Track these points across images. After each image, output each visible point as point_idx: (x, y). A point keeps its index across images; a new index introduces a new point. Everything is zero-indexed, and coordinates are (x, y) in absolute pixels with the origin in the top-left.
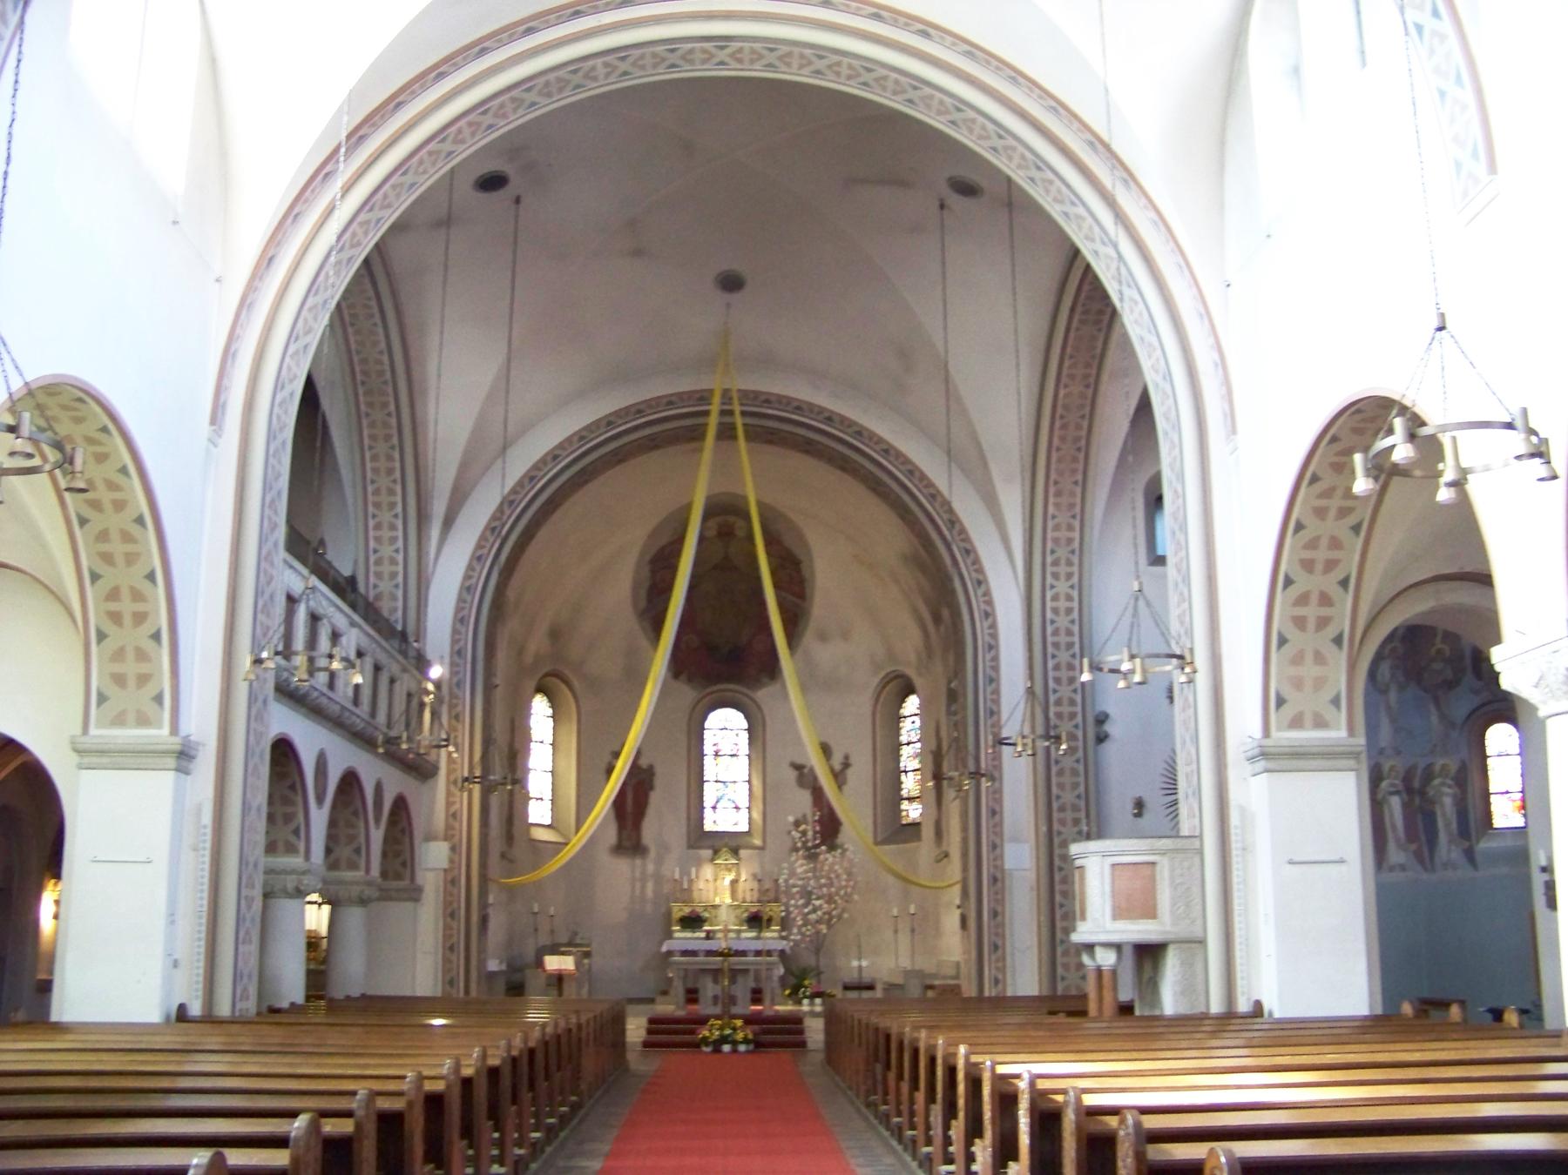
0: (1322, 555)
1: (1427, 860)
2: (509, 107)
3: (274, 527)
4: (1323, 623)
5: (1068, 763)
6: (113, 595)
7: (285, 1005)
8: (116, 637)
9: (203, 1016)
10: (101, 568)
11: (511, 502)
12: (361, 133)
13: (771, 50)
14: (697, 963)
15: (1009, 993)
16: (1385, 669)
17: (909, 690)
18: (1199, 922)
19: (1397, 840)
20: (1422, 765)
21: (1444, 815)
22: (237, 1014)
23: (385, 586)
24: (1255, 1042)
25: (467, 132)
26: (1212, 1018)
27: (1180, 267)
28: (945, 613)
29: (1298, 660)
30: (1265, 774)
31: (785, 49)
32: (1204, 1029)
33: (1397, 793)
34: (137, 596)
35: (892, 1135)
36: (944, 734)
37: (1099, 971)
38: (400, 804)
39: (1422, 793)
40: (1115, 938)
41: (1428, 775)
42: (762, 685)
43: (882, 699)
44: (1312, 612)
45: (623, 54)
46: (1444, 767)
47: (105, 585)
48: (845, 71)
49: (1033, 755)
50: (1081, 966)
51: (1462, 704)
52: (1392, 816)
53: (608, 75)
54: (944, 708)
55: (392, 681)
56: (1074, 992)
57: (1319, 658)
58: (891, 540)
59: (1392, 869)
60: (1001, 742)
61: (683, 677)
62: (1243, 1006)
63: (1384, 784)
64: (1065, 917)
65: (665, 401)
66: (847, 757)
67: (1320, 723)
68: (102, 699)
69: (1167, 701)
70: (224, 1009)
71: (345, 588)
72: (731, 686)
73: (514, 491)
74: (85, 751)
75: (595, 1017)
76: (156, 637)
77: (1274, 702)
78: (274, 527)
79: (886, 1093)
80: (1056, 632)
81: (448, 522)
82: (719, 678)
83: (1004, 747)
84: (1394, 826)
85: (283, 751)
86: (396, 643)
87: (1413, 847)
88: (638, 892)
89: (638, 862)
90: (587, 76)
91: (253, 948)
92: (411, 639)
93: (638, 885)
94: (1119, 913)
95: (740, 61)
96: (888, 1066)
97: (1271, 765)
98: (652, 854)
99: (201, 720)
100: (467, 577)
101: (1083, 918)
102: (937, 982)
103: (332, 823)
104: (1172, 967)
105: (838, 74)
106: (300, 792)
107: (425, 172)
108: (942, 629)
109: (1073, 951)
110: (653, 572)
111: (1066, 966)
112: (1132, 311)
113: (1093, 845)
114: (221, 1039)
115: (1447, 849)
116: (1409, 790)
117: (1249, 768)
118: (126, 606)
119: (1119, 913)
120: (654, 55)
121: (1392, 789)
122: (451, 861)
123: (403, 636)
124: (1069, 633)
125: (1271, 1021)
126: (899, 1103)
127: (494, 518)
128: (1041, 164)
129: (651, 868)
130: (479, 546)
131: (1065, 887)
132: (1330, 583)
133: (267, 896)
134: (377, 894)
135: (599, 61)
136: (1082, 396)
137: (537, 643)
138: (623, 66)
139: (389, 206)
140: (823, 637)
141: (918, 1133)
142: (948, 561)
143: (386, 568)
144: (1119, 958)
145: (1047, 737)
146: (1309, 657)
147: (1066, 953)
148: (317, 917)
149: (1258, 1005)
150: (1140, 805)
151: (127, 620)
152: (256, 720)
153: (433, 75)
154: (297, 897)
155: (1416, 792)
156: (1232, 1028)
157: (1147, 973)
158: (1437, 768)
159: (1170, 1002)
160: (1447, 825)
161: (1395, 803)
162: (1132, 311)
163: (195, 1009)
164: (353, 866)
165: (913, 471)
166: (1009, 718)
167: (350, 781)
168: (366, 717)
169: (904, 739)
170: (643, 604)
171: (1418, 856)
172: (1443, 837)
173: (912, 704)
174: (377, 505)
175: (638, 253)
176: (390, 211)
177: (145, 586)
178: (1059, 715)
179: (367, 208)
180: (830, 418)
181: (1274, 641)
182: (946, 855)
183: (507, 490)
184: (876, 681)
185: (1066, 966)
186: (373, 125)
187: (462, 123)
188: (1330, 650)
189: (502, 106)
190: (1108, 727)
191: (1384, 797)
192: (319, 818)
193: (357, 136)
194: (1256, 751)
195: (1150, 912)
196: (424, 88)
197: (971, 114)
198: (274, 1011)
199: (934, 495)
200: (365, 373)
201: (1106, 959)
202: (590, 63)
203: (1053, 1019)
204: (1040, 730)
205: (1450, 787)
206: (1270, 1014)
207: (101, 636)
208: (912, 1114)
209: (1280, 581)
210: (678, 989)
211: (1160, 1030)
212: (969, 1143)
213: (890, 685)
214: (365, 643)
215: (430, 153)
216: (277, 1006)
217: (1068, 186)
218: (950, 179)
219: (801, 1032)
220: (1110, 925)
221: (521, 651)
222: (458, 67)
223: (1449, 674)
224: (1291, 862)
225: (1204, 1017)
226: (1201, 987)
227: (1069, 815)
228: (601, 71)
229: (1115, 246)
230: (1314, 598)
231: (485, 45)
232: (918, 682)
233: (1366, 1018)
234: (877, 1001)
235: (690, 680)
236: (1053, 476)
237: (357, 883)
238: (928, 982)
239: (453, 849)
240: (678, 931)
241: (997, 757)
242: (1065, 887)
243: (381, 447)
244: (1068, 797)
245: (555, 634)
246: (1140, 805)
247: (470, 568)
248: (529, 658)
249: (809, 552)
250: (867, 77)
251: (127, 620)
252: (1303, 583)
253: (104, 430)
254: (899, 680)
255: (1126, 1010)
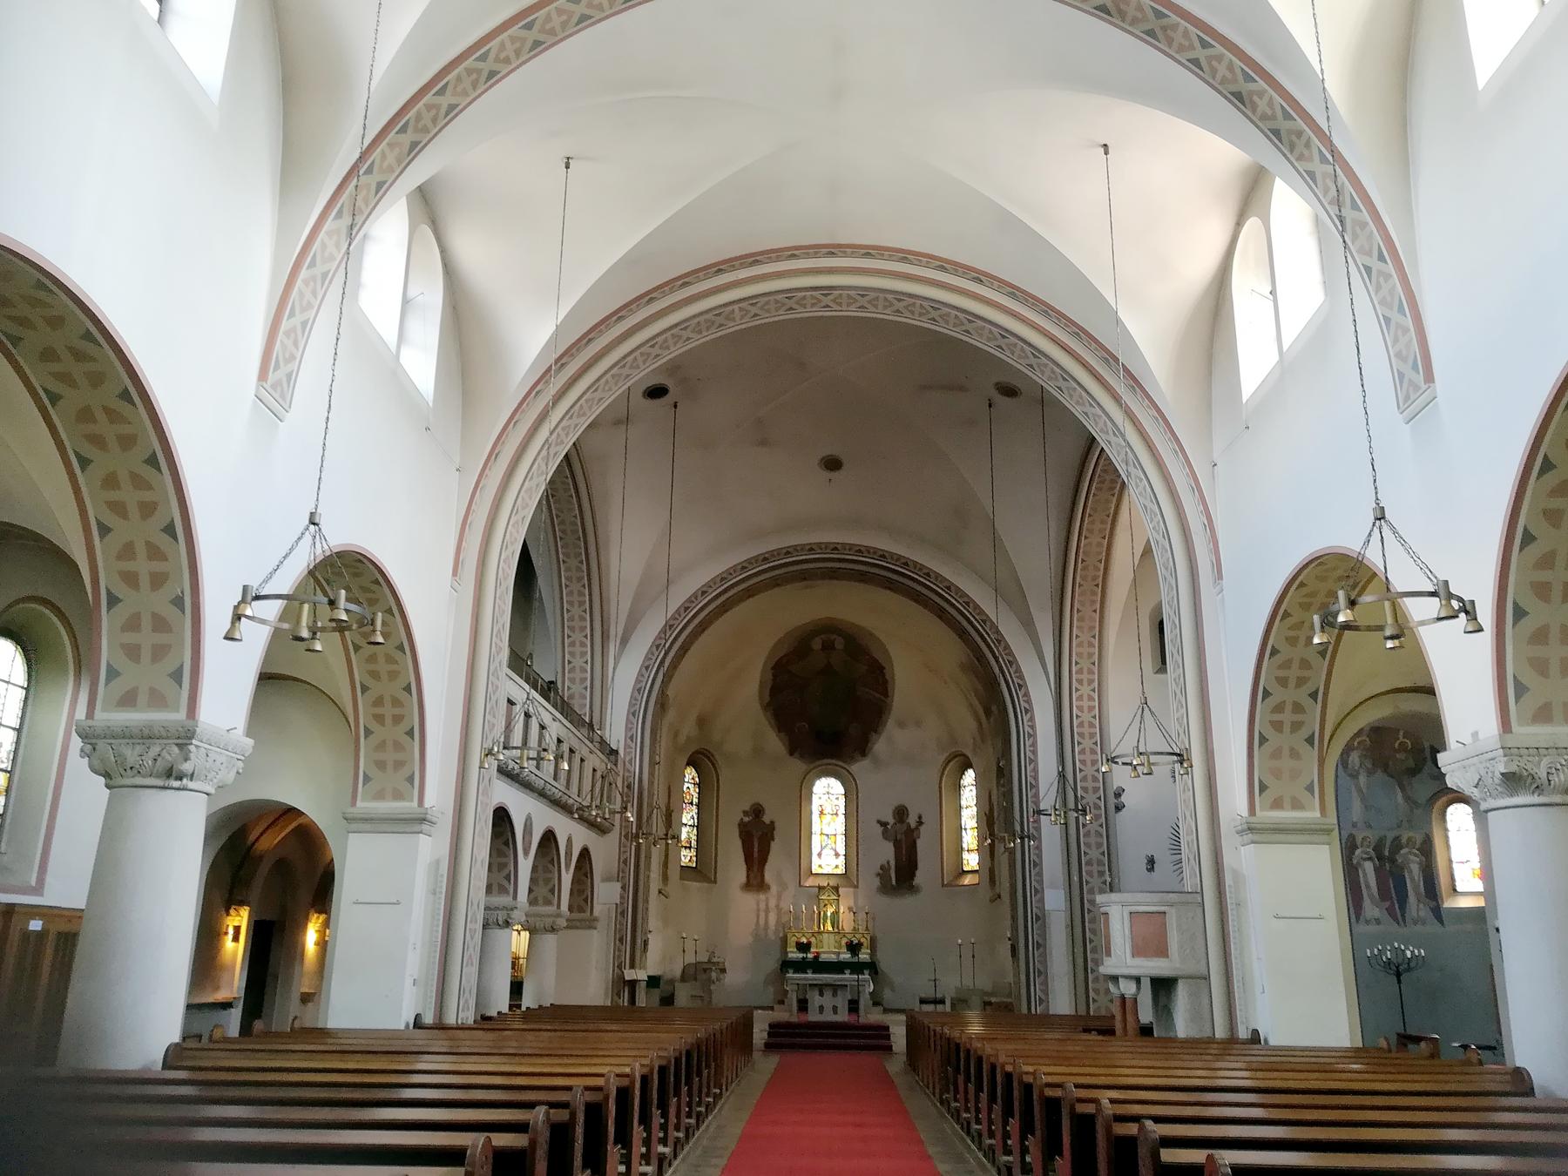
0: (1294, 673)
1: (1400, 920)
2: (671, 342)
3: (499, 650)
4: (1296, 726)
5: (1094, 827)
6: (379, 702)
7: (494, 1013)
8: (380, 732)
9: (434, 1024)
10: (370, 682)
11: (671, 626)
12: (563, 361)
13: (863, 296)
14: (805, 979)
15: (1051, 1013)
16: (1355, 757)
17: (971, 766)
18: (1204, 962)
19: (1371, 896)
20: (1390, 836)
21: (1412, 879)
22: (460, 1022)
23: (577, 688)
24: (1254, 1066)
25: (640, 360)
26: (1217, 1043)
27: (1176, 452)
28: (994, 708)
29: (1277, 754)
30: (1252, 845)
31: (873, 295)
32: (1212, 1051)
33: (1370, 859)
34: (396, 702)
35: (962, 1128)
36: (994, 798)
37: (1123, 998)
38: (585, 854)
39: (1393, 861)
40: (1134, 972)
41: (1397, 845)
42: (857, 761)
43: (946, 772)
44: (1287, 717)
45: (754, 301)
46: (1409, 839)
47: (372, 695)
48: (917, 310)
49: (1066, 824)
50: (1108, 991)
51: (1422, 788)
52: (1365, 875)
53: (742, 317)
54: (995, 782)
55: (582, 760)
56: (1103, 1013)
57: (1294, 754)
58: (950, 651)
59: (1367, 922)
60: (1039, 812)
61: (796, 754)
62: (1243, 1033)
63: (1358, 852)
64: (1094, 950)
65: (785, 551)
66: (920, 817)
67: (1297, 805)
68: (367, 779)
69: (1172, 779)
70: (451, 1019)
71: (548, 690)
72: (834, 761)
73: (673, 618)
74: (350, 819)
75: (732, 1023)
76: (410, 733)
77: (1257, 787)
78: (499, 650)
79: (956, 1091)
80: (1081, 725)
81: (624, 641)
82: (824, 755)
83: (1042, 816)
84: (1368, 887)
85: (501, 817)
86: (585, 731)
87: (1387, 904)
88: (762, 922)
89: (762, 897)
90: (727, 318)
91: (474, 969)
92: (596, 727)
93: (762, 915)
94: (1137, 952)
95: (840, 304)
96: (957, 1071)
97: (1256, 837)
98: (774, 889)
99: (438, 791)
100: (638, 681)
101: (1109, 954)
102: (993, 1000)
103: (534, 869)
104: (1182, 995)
105: (912, 313)
106: (511, 846)
107: (610, 389)
108: (992, 720)
109: (1101, 979)
110: (775, 676)
111: (1096, 991)
112: (1137, 486)
113: (1114, 896)
114: (446, 1043)
115: (1416, 906)
116: (1380, 857)
117: (1238, 839)
118: (388, 710)
119: (1137, 952)
120: (777, 302)
121: (1365, 856)
122: (622, 897)
123: (591, 726)
124: (1091, 725)
125: (1266, 1047)
126: (967, 1100)
127: (658, 637)
128: (1067, 376)
129: (772, 903)
130: (647, 658)
131: (1092, 926)
132: (1302, 696)
133: (486, 926)
134: (565, 924)
135: (736, 307)
136: (1100, 545)
137: (689, 729)
138: (754, 310)
139: (584, 414)
140: (901, 724)
141: (983, 1127)
142: (997, 670)
143: (578, 675)
144: (1139, 988)
145: (1076, 810)
146: (1286, 752)
147: (1096, 980)
148: (519, 941)
149: (1255, 1032)
150: (1151, 863)
151: (388, 721)
152: (483, 794)
153: (615, 318)
154: (507, 927)
155: (1388, 859)
156: (1235, 1052)
157: (1163, 1000)
158: (1404, 840)
159: (1183, 1027)
160: (1416, 888)
161: (1369, 867)
162: (1137, 486)
163: (428, 1019)
164: (548, 902)
165: (969, 602)
166: (1043, 798)
167: (549, 837)
168: (563, 789)
169: (963, 803)
170: (767, 699)
171: (1390, 911)
172: (1412, 898)
173: (969, 777)
174: (572, 629)
175: (763, 443)
176: (584, 418)
177: (403, 695)
178: (1085, 789)
179: (567, 417)
180: (906, 563)
181: (1256, 740)
182: (999, 897)
183: (669, 616)
184: (942, 758)
185: (1096, 991)
186: (572, 355)
187: (637, 353)
188: (1304, 749)
189: (666, 341)
190: (1123, 798)
191: (1358, 863)
192: (525, 865)
193: (561, 362)
194: (1245, 826)
195: (1162, 952)
196: (608, 328)
197: (1013, 340)
198: (485, 1018)
199: (985, 620)
200: (563, 532)
201: (1128, 988)
202: (730, 308)
203: (1085, 1036)
204: (1071, 805)
205: (1416, 855)
206: (1266, 1041)
207: (368, 732)
208: (978, 1111)
209: (1259, 693)
210: (793, 999)
211: (1176, 1050)
212: (1023, 1138)
213: (951, 764)
214: (563, 733)
215: (613, 376)
216: (488, 1014)
217: (1058, 365)
218: (997, 384)
219: (888, 1037)
220: (1130, 960)
221: (676, 735)
222: (633, 312)
223: (1411, 763)
224: (1277, 917)
225: (1211, 1040)
226: (1207, 1016)
227: (1095, 868)
228: (737, 314)
229: (1123, 436)
230: (1289, 707)
231: (652, 296)
232: (974, 760)
233: (1347, 1050)
234: (945, 1014)
235: (802, 757)
236: (1076, 606)
237: (549, 916)
238: (986, 999)
239: (623, 888)
240: (792, 952)
241: (1037, 821)
242: (1092, 926)
243: (575, 587)
244: (1094, 854)
245: (702, 722)
246: (1151, 863)
247: (640, 674)
248: (682, 739)
249: (891, 662)
250: (934, 314)
251: (388, 721)
252: (1278, 694)
253: (377, 582)
254: (962, 757)
255: (1146, 1031)
